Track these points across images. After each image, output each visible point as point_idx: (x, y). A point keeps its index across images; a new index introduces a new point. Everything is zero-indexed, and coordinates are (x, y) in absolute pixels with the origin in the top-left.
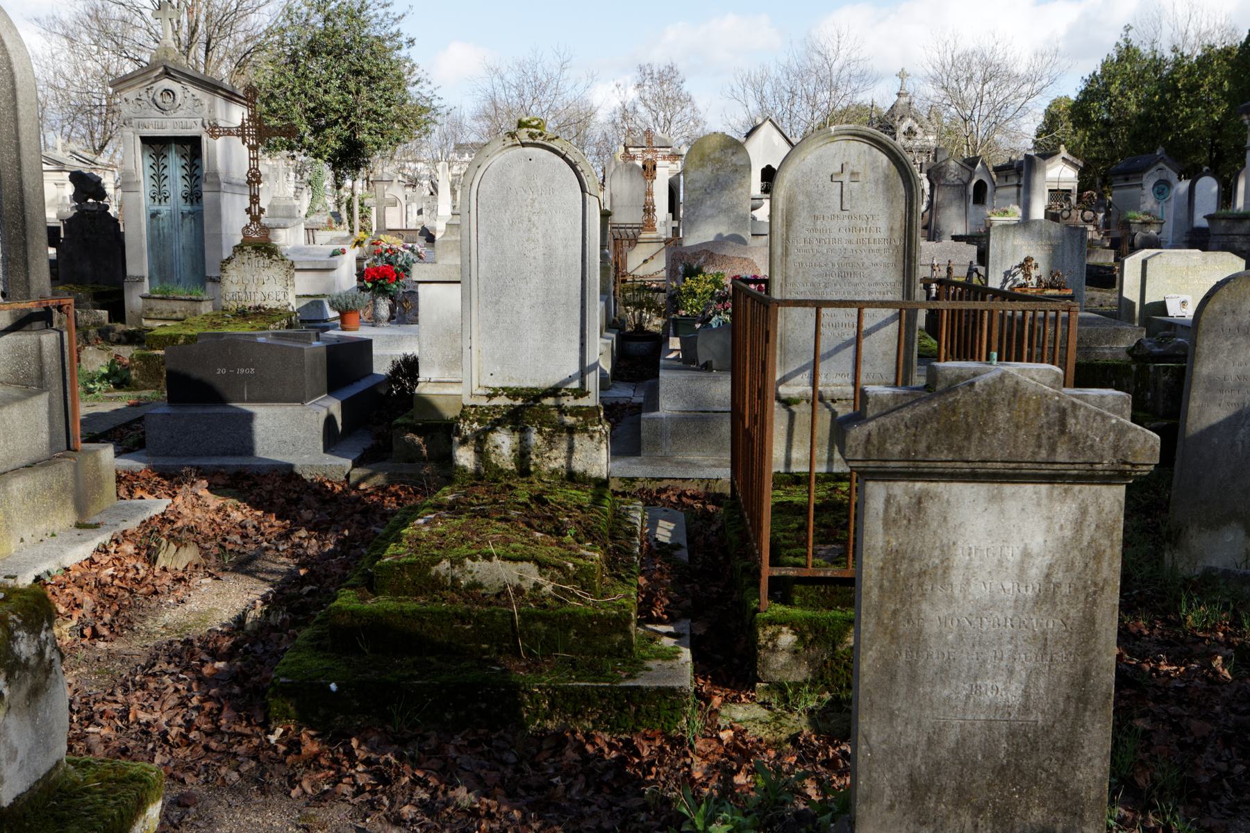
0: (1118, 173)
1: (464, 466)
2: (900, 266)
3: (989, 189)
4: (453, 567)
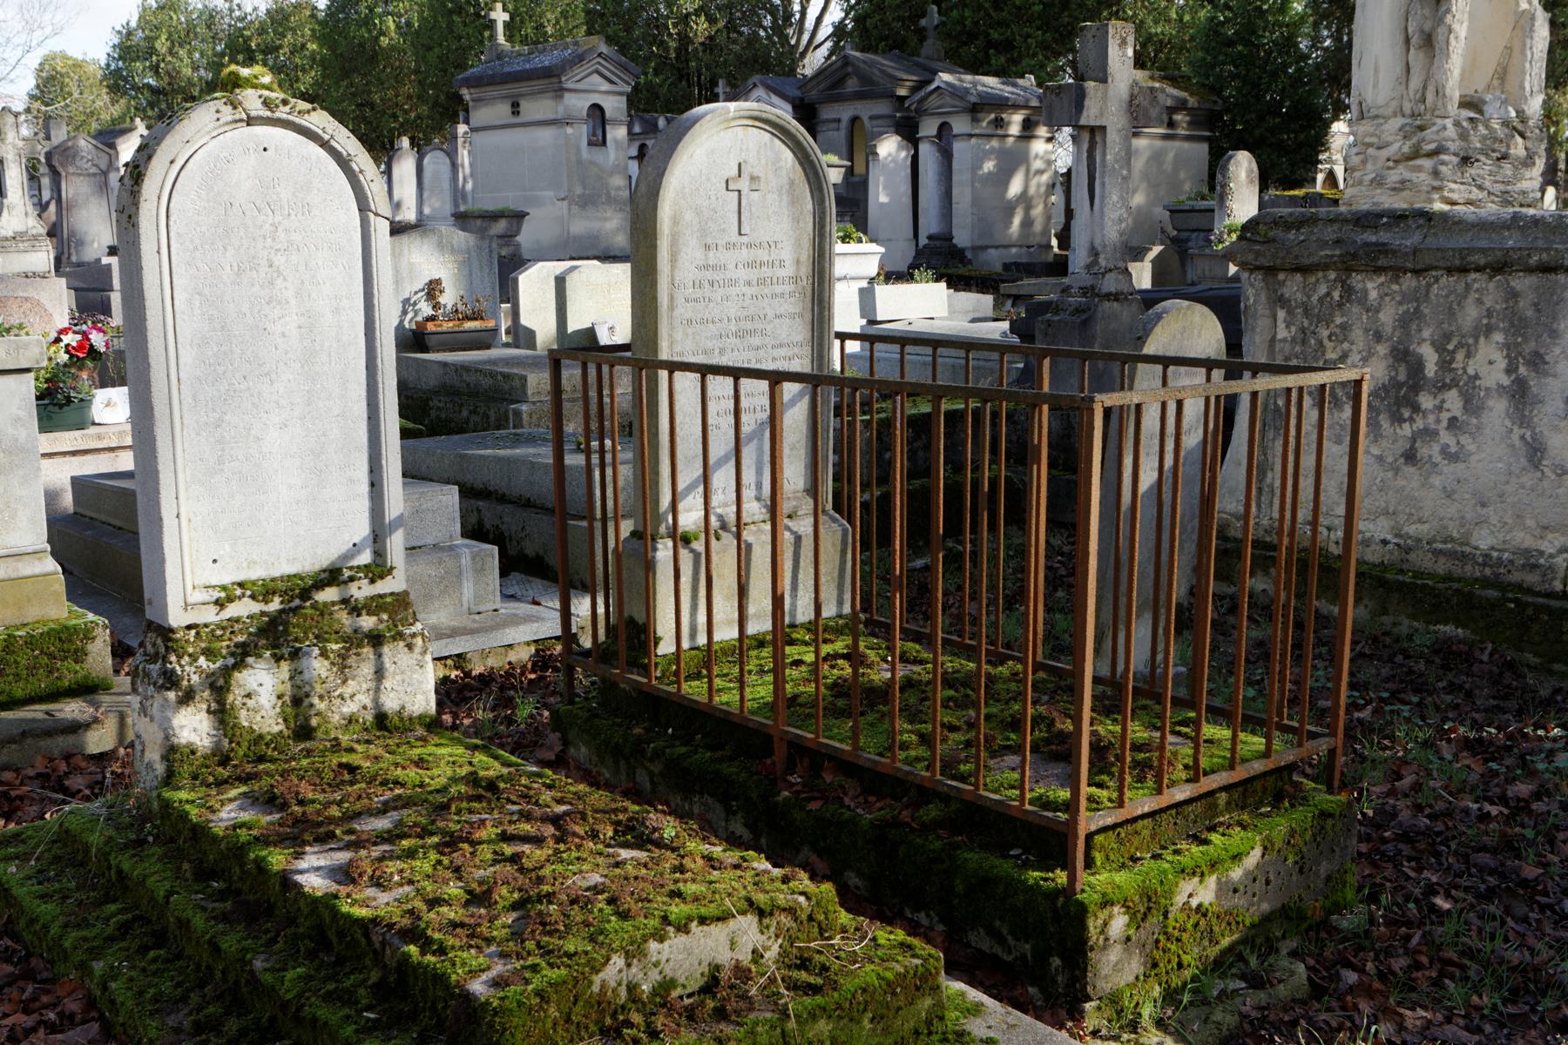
1: (188, 745)
2: (808, 316)
4: (629, 965)
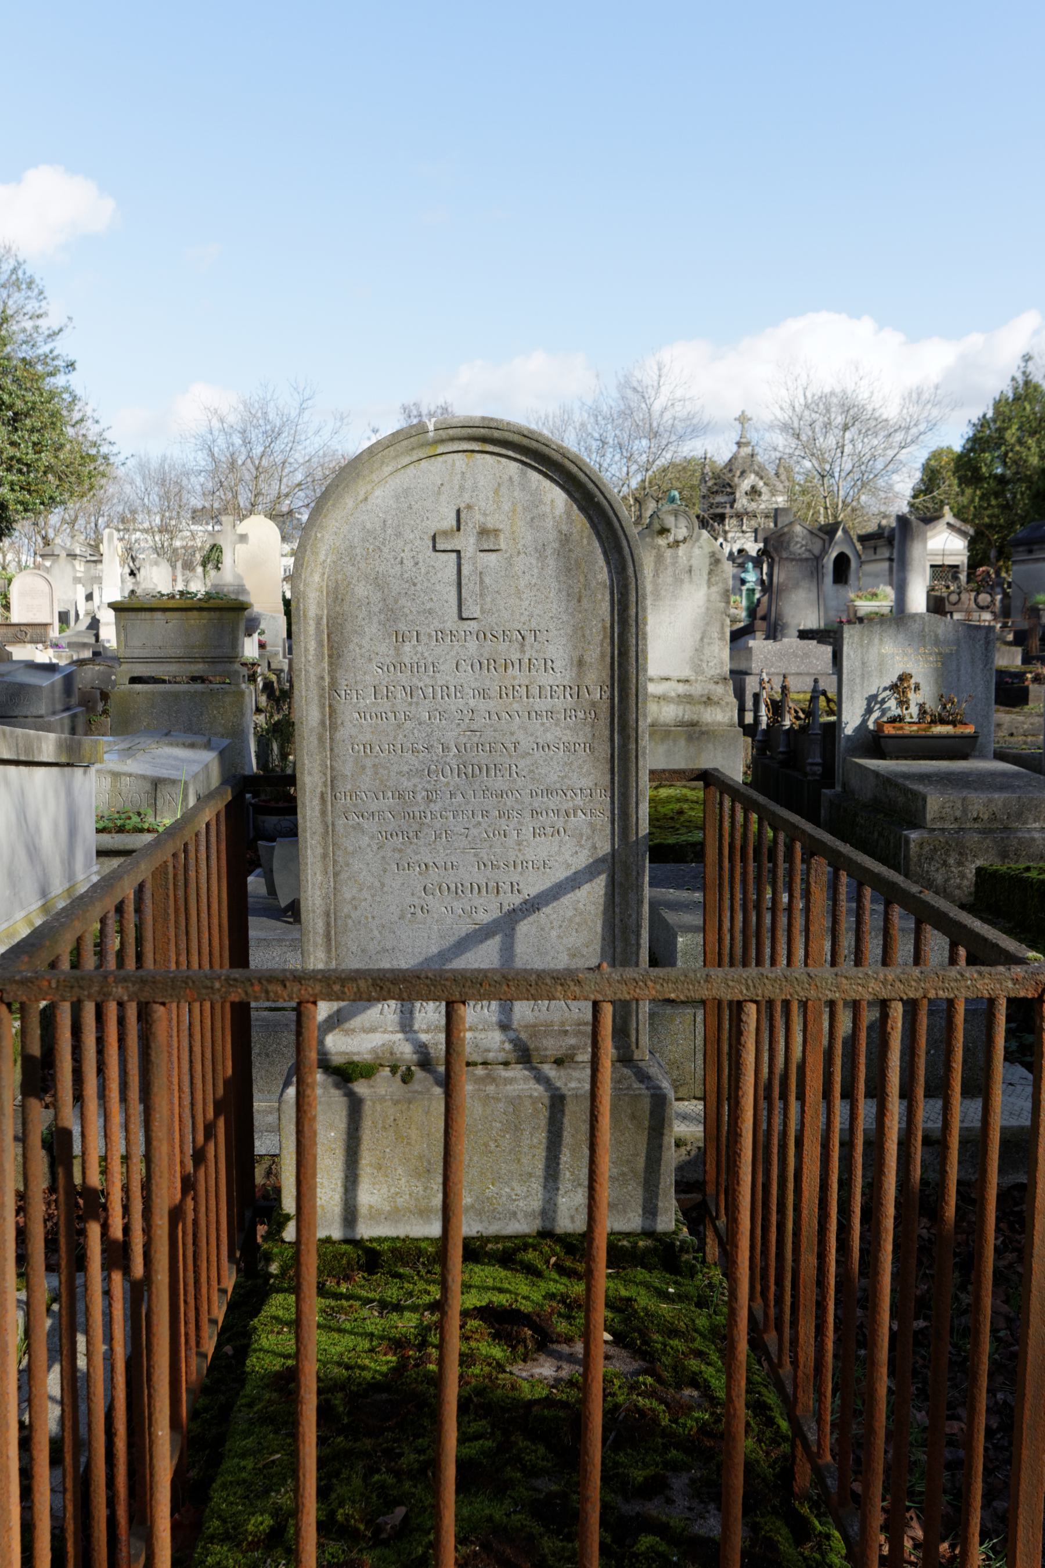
0: (1018, 543)
2: (603, 750)
3: (854, 564)
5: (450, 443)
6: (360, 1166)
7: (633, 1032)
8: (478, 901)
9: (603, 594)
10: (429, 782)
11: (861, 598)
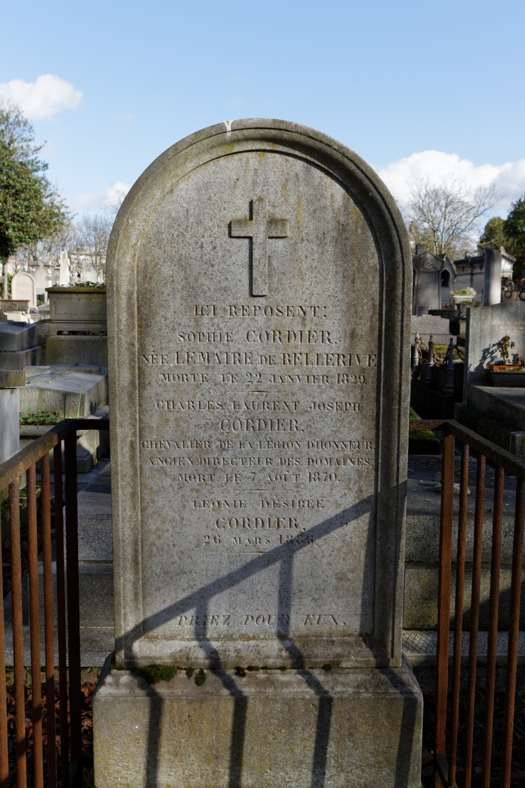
2: (370, 409)
3: (451, 276)
5: (245, 143)
6: (160, 753)
7: (390, 644)
8: (262, 533)
9: (374, 277)
10: (223, 433)
11: (457, 294)
